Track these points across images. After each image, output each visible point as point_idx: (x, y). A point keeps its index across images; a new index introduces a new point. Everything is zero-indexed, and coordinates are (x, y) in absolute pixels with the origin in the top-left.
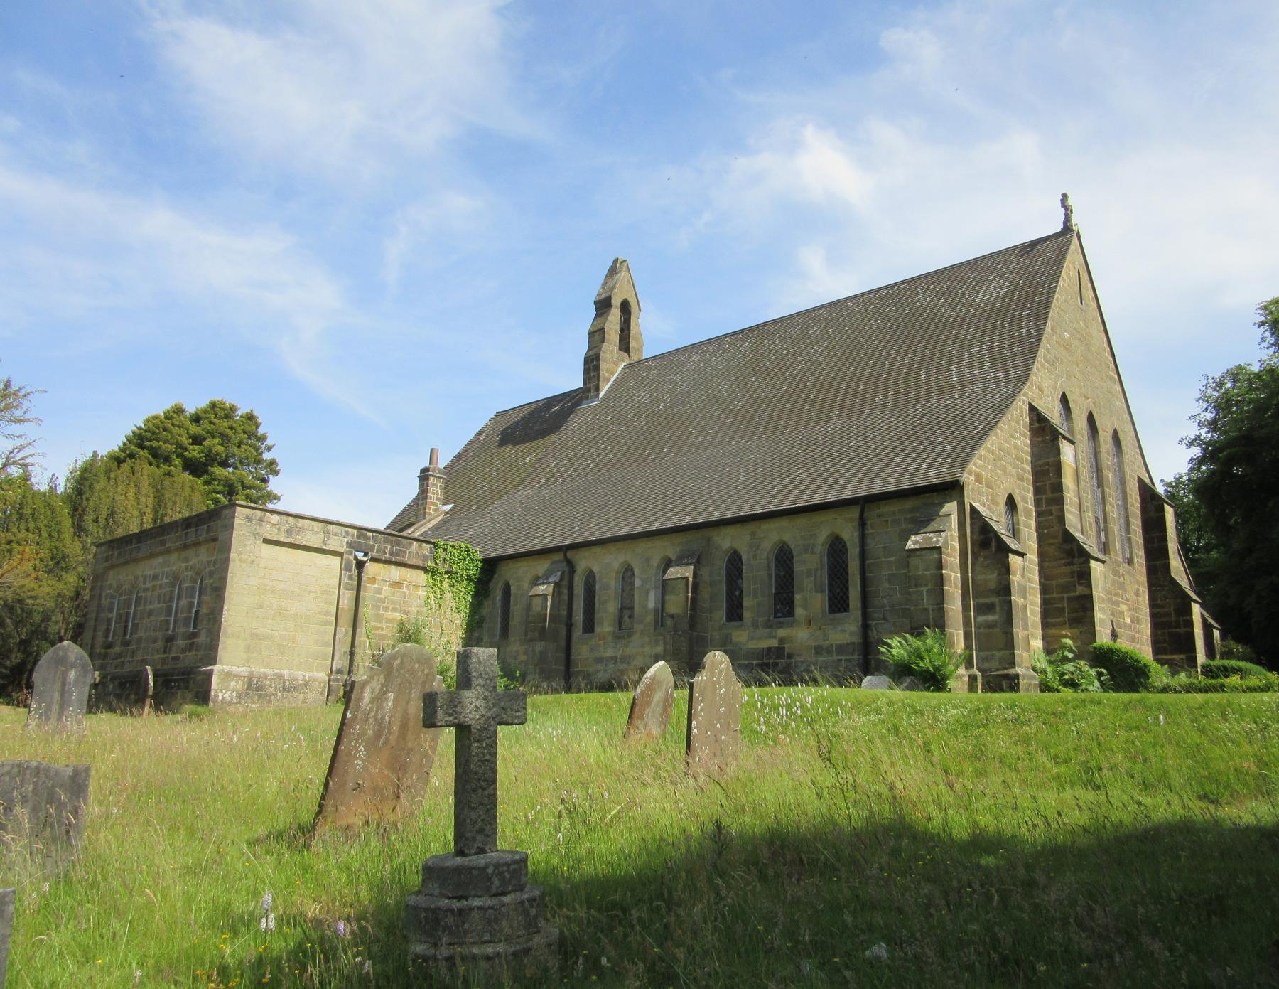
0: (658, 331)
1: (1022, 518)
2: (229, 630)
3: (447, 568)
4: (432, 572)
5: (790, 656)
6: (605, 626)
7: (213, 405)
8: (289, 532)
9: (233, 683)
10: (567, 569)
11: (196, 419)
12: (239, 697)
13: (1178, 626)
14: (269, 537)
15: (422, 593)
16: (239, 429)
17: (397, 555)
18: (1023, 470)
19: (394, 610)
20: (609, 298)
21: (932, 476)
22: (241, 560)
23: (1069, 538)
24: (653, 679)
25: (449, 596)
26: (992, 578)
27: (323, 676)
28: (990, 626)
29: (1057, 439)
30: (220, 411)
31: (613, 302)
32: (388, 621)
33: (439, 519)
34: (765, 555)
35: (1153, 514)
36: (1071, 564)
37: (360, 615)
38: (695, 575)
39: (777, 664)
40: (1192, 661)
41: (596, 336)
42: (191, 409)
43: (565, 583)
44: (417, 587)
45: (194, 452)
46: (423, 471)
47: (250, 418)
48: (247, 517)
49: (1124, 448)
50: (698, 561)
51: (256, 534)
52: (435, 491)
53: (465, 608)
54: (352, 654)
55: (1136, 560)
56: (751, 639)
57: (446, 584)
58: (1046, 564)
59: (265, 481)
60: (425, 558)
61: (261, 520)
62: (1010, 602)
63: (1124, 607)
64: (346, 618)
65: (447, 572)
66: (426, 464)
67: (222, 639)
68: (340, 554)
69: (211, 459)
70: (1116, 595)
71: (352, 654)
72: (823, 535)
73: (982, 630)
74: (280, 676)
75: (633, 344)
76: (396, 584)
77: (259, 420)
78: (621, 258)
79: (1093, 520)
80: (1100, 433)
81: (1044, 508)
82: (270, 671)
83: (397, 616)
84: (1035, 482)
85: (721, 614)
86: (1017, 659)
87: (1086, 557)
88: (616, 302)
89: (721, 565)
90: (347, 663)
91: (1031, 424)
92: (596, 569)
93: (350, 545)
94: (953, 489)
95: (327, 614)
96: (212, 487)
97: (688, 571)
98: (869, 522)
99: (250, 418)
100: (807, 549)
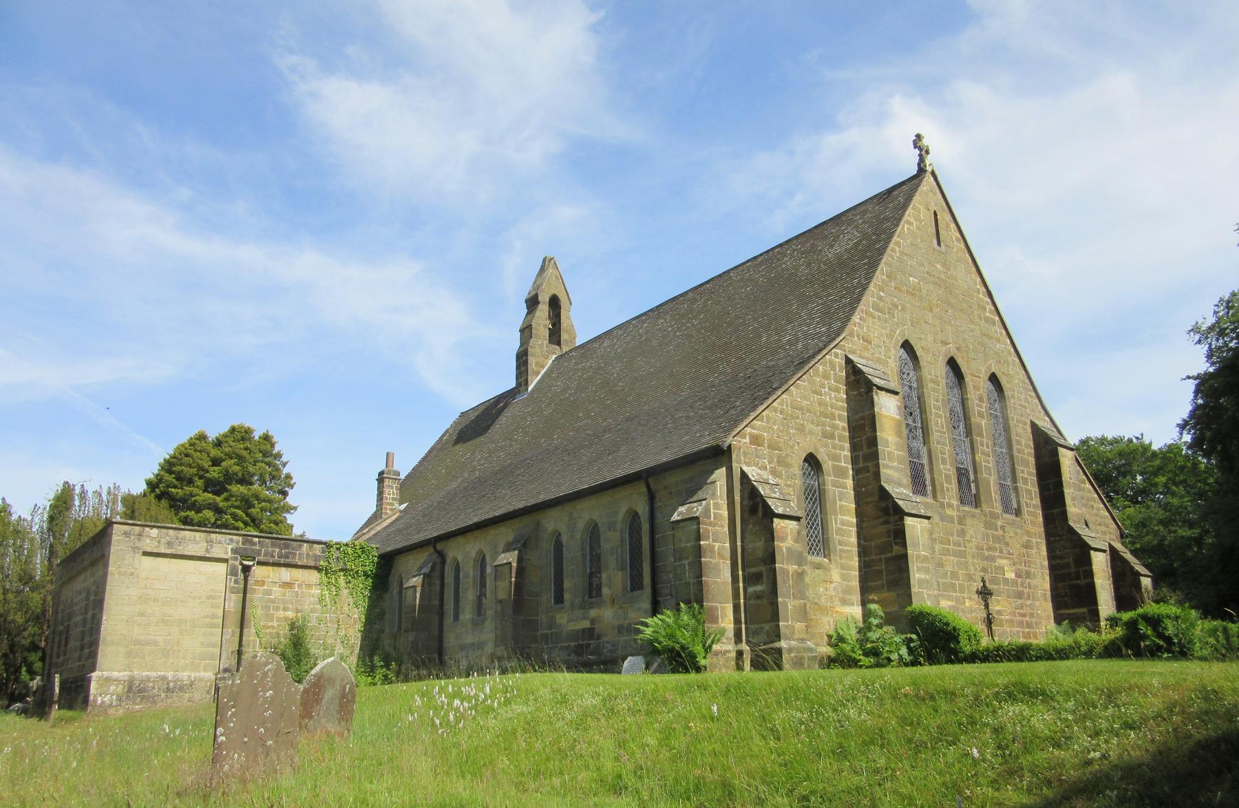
0: (584, 324)
1: (829, 479)
2: (108, 638)
3: (341, 565)
4: (326, 571)
5: (599, 637)
6: (467, 615)
7: (233, 430)
8: (169, 544)
9: (112, 688)
10: (439, 560)
11: (218, 443)
12: (120, 699)
13: (1078, 578)
15: (316, 591)
16: (192, 452)
17: (286, 557)
18: (834, 427)
19: (285, 609)
20: (536, 296)
21: (705, 442)
22: (119, 573)
23: (884, 495)
24: (320, 676)
25: (345, 592)
26: (758, 545)
27: (210, 675)
28: (758, 596)
29: (869, 391)
30: (240, 434)
31: (540, 299)
32: (279, 619)
33: (394, 518)
34: (579, 536)
36: (887, 522)
37: (247, 616)
38: (520, 560)
39: (589, 645)
40: (1095, 614)
41: (526, 331)
42: (212, 435)
43: (437, 573)
44: (309, 586)
45: (214, 473)
46: (381, 473)
47: (266, 438)
48: (125, 533)
49: (1007, 393)
50: (524, 545)
51: (135, 549)
52: (391, 492)
53: (364, 604)
54: (240, 653)
55: (1025, 509)
56: (570, 621)
57: (342, 581)
58: (865, 525)
59: (285, 494)
60: (317, 558)
61: (140, 535)
62: (775, 570)
63: (1004, 562)
64: (234, 619)
65: (341, 570)
66: (382, 467)
67: (101, 647)
68: (226, 561)
69: (229, 478)
70: (989, 549)
71: (240, 653)
72: (623, 510)
73: (752, 602)
74: (164, 678)
75: (564, 336)
76: (288, 585)
77: (275, 439)
78: (549, 256)
81: (861, 465)
82: (153, 674)
83: (290, 614)
84: (852, 438)
85: (548, 598)
86: (783, 630)
87: (900, 514)
88: (544, 298)
89: (547, 547)
90: (234, 662)
91: (847, 377)
92: (460, 558)
93: (235, 551)
94: (719, 455)
95: (214, 616)
96: (229, 503)
97: (512, 557)
98: (657, 495)
99: (266, 438)
100: (611, 527)
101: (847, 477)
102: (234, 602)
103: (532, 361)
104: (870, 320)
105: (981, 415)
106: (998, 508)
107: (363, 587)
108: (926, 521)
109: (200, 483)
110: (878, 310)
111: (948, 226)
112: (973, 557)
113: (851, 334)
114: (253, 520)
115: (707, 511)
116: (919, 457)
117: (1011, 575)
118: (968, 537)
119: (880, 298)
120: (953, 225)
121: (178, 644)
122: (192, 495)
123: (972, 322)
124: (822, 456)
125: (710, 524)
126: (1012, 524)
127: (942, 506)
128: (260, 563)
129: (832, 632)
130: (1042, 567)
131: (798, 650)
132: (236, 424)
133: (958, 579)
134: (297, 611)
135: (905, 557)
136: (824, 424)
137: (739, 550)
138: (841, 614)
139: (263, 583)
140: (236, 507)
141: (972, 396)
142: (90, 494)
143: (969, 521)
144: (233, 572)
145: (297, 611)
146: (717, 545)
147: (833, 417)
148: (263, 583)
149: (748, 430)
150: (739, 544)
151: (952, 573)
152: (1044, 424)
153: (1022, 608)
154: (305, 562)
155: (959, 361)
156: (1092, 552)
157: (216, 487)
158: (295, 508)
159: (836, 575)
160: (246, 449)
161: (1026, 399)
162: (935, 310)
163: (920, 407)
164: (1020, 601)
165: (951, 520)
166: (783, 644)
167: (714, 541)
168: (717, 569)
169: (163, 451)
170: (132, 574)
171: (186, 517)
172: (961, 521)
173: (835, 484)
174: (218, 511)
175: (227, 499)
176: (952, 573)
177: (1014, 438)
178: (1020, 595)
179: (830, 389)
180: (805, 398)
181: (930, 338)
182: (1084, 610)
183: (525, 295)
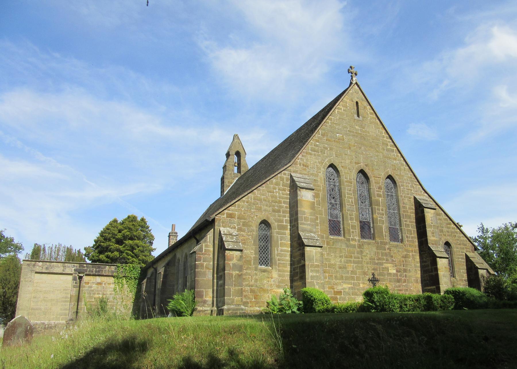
2: (20, 308)
3: (123, 274)
4: (117, 277)
7: (129, 217)
8: (47, 268)
11: (123, 223)
13: (432, 271)
14: (38, 271)
15: (113, 286)
16: (110, 227)
18: (281, 207)
22: (25, 281)
25: (126, 286)
29: (296, 189)
30: (132, 219)
31: (230, 153)
35: (420, 215)
42: (120, 220)
43: (153, 277)
44: (109, 284)
45: (119, 236)
47: (143, 220)
57: (124, 281)
60: (113, 272)
61: (34, 265)
64: (75, 298)
65: (123, 277)
66: (170, 231)
68: (71, 274)
69: (125, 237)
71: (77, 312)
74: (43, 324)
76: (100, 284)
77: (146, 220)
79: (357, 225)
80: (372, 179)
83: (101, 296)
86: (226, 301)
88: (233, 153)
90: (75, 316)
93: (75, 270)
95: (66, 298)
99: (143, 220)
101: (287, 229)
102: (75, 292)
103: (226, 181)
104: (309, 156)
105: (379, 196)
106: (387, 239)
107: (134, 283)
108: (319, 249)
109: (113, 240)
110: (315, 151)
111: (365, 107)
112: (367, 263)
113: (296, 164)
114: (136, 255)
115: (201, 249)
116: (337, 217)
117: (393, 271)
118: (364, 254)
119: (317, 146)
120: (369, 107)
121: (50, 309)
122: (109, 246)
123: (377, 152)
124: (271, 220)
125: (203, 254)
126: (396, 247)
127: (348, 240)
128: (86, 275)
129: (269, 301)
130: (416, 266)
131: (234, 310)
132: (130, 215)
133: (356, 274)
134: (104, 294)
135: (304, 266)
136: (274, 206)
137: (216, 265)
138: (276, 292)
139: (88, 283)
140: (128, 250)
141: (374, 186)
142: (47, 249)
143: (366, 246)
144: (74, 279)
145: (104, 294)
146: (205, 263)
147: (280, 202)
148: (88, 283)
149: (226, 211)
150: (216, 262)
151: (352, 271)
152: (422, 198)
153: (400, 286)
154: (107, 274)
155: (367, 171)
156: (438, 259)
157: (119, 242)
158: (155, 249)
159: (275, 274)
160: (133, 225)
161: (412, 186)
162: (352, 148)
163: (339, 194)
164: (398, 284)
165: (354, 246)
166: (225, 307)
167: (203, 261)
168: (205, 274)
169: (101, 228)
170: (30, 281)
171: (107, 255)
172: (360, 246)
173: (278, 233)
174: (121, 252)
175: (124, 247)
176: (352, 271)
177: (401, 205)
178: (399, 281)
179: (279, 189)
180: (263, 195)
181: (348, 161)
182: (434, 287)
183: (226, 152)
